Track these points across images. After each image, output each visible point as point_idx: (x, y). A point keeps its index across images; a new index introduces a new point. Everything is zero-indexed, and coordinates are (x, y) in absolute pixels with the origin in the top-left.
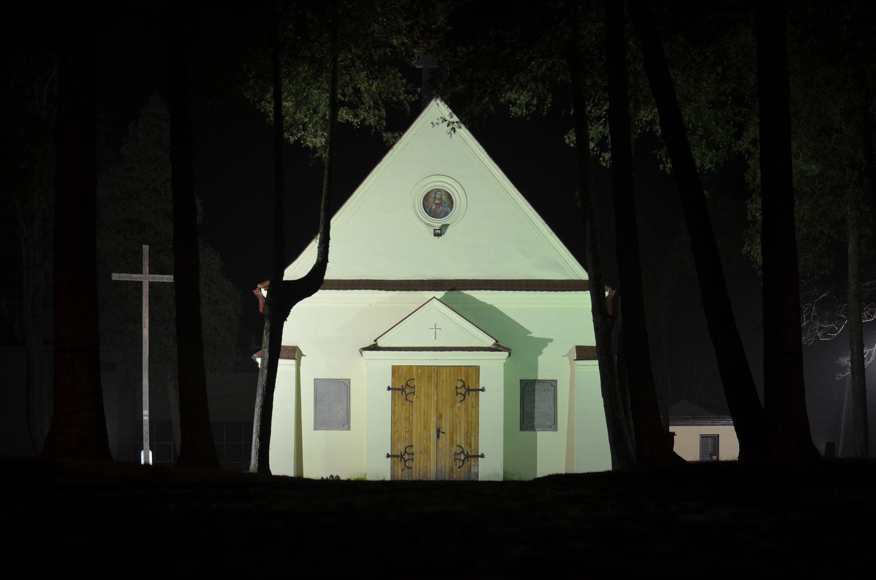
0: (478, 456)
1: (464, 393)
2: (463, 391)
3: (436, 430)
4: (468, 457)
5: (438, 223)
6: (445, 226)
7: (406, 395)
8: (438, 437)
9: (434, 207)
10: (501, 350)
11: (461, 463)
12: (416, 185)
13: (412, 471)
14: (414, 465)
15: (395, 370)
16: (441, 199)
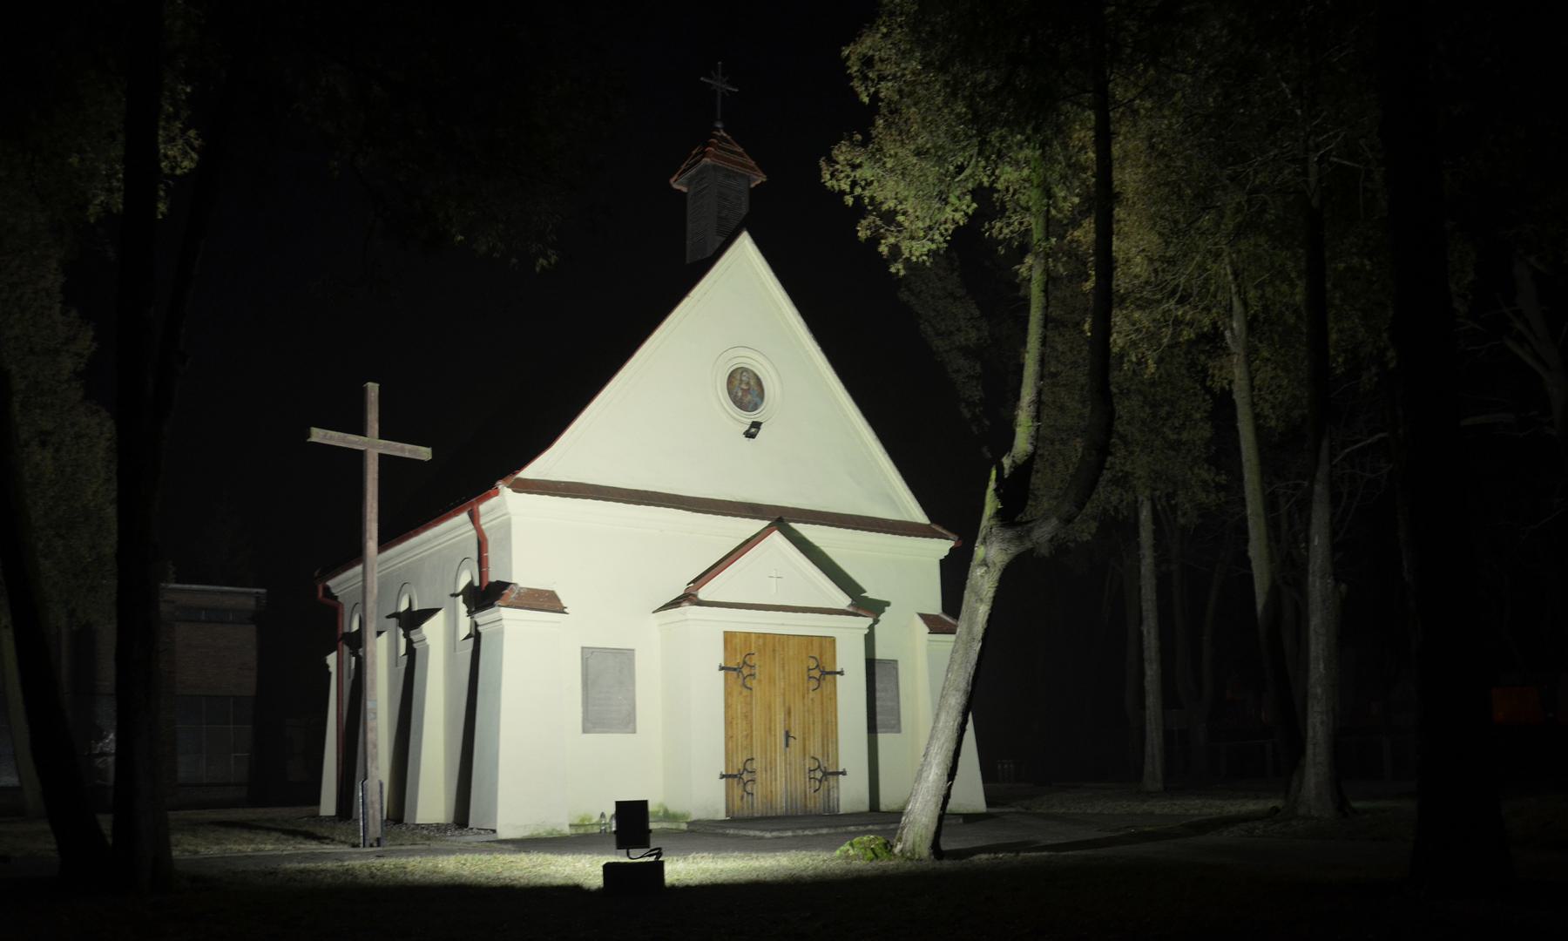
0: (837, 773)
1: (818, 677)
2: (816, 674)
3: (783, 732)
4: (826, 774)
5: (747, 418)
6: (756, 425)
7: (744, 678)
8: (787, 745)
9: (740, 394)
10: (864, 614)
11: (817, 783)
12: (717, 359)
13: (753, 799)
14: (758, 790)
15: (729, 637)
16: (748, 384)
